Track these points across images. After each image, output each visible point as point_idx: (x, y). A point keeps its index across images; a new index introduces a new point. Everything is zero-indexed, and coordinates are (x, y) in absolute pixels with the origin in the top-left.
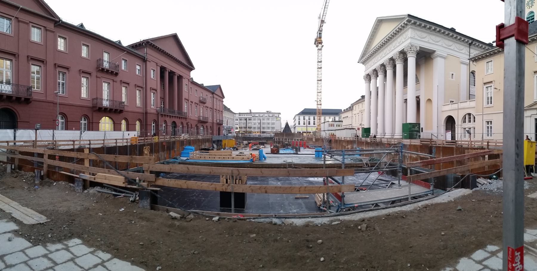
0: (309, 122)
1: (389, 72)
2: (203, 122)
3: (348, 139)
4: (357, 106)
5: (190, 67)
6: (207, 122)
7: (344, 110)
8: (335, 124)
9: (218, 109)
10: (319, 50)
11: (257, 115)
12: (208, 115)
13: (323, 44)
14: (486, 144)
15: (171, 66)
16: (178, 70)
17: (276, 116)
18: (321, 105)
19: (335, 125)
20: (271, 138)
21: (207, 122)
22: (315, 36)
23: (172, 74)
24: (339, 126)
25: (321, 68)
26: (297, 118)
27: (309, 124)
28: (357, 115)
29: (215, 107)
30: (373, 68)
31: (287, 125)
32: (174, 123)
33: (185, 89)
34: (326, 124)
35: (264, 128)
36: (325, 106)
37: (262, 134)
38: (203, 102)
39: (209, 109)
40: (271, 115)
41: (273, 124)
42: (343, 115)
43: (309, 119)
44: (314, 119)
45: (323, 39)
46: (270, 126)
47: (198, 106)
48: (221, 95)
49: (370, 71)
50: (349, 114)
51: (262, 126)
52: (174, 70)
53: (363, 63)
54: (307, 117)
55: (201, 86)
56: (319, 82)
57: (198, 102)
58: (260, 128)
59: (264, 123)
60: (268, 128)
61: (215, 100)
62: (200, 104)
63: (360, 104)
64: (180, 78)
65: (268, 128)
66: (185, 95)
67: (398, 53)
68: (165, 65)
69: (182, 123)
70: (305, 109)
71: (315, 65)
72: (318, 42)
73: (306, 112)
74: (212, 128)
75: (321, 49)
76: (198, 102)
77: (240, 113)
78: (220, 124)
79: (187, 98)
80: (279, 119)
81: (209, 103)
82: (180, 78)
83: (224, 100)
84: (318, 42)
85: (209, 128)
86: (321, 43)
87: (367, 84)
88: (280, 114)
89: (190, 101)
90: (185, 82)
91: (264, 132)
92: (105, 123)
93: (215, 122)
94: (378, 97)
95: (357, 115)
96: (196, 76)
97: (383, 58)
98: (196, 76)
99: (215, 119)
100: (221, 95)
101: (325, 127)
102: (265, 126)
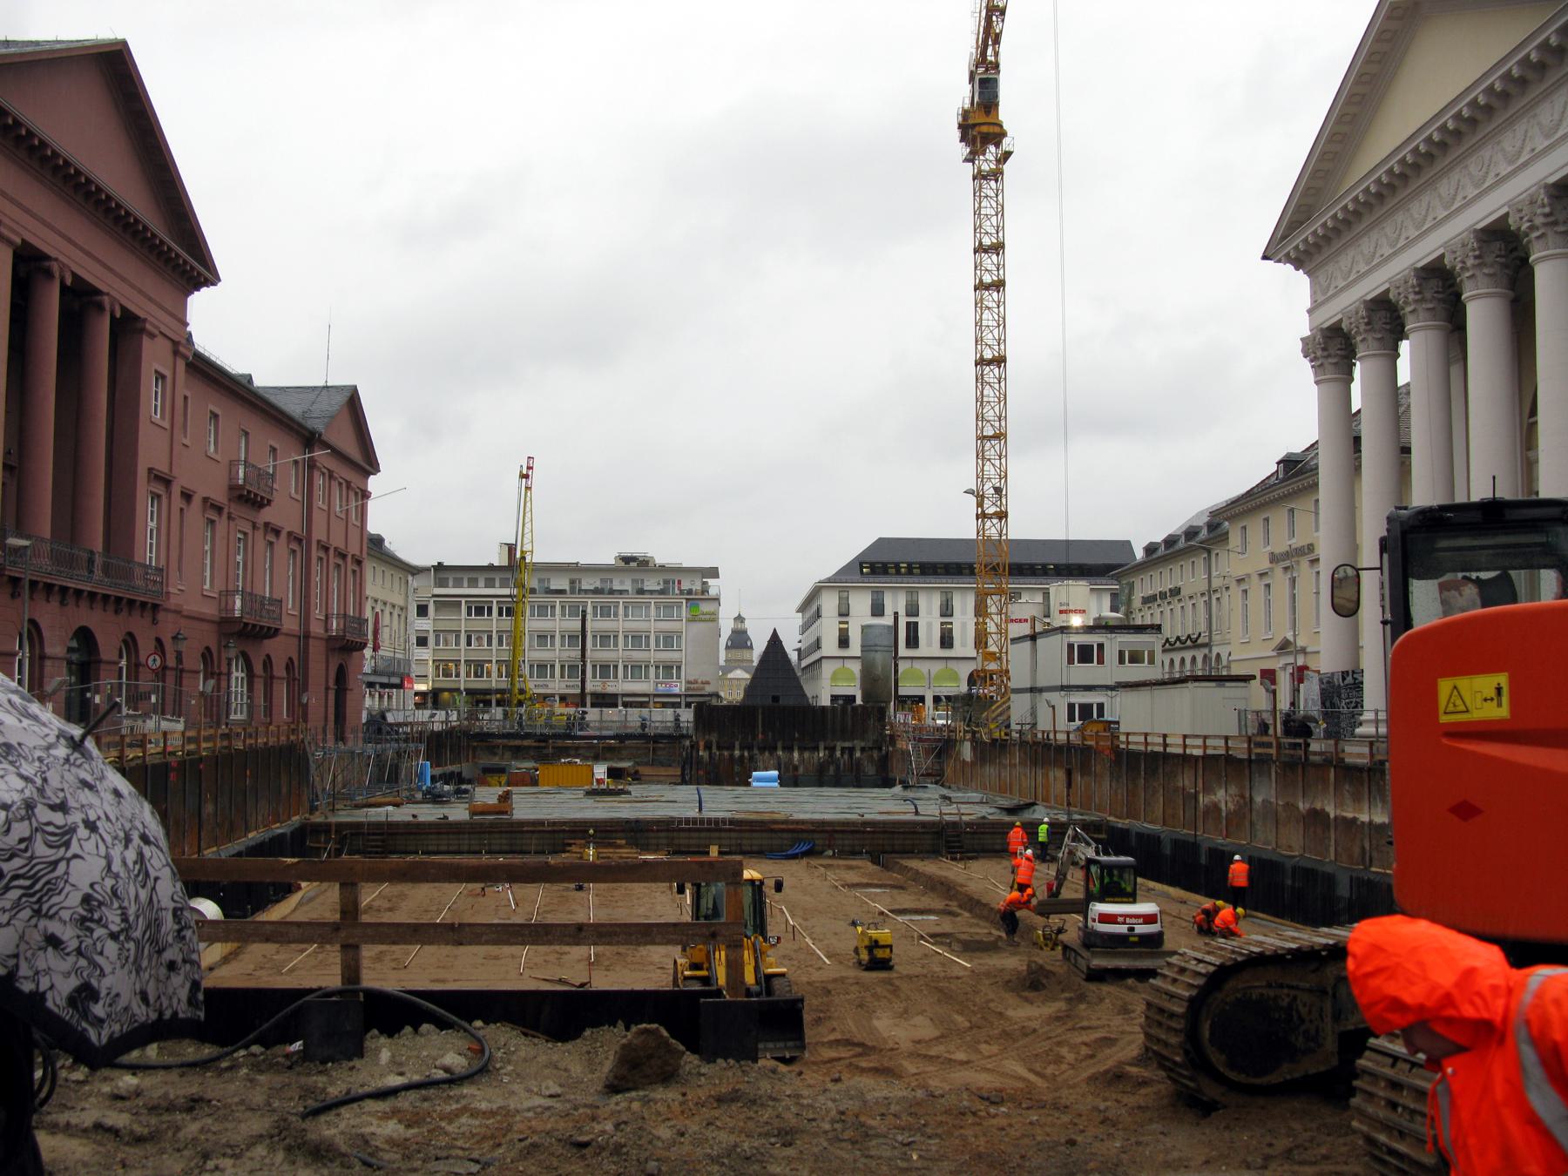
0: (912, 629)
1: (1483, 316)
2: (245, 633)
3: (1216, 747)
4: (1255, 526)
5: (189, 263)
6: (273, 633)
7: (1150, 549)
8: (1113, 644)
9: (337, 541)
10: (980, 176)
11: (560, 583)
12: (276, 579)
13: (1006, 144)
14: (1161, 740)
15: (79, 250)
16: (121, 280)
17: (688, 589)
18: (1002, 515)
19: (1111, 654)
20: (673, 738)
21: (273, 633)
22: (961, 94)
23: (81, 300)
24: (1135, 658)
25: (999, 285)
26: (829, 603)
27: (912, 641)
28: (1256, 587)
29: (319, 533)
30: (1372, 286)
31: (775, 641)
32: (85, 636)
33: (152, 403)
34: (1052, 647)
35: (605, 670)
36: (1029, 522)
37: (593, 714)
38: (249, 499)
39: (282, 546)
40: (652, 584)
41: (668, 640)
42: (1145, 586)
43: (913, 610)
44: (947, 611)
45: (1007, 113)
46: (654, 655)
47: (222, 525)
48: (353, 452)
49: (1349, 301)
50: (1189, 576)
51: (595, 654)
52: (93, 275)
53: (1298, 263)
54: (895, 603)
55: (235, 390)
56: (991, 373)
57: (220, 496)
58: (577, 669)
59: (605, 639)
60: (636, 670)
61: (319, 481)
62: (236, 509)
63: (1279, 517)
64: (127, 327)
65: (636, 670)
66: (151, 451)
67: (1543, 197)
68: (45, 241)
69: (130, 642)
70: (882, 543)
71: (962, 271)
72: (981, 129)
73: (885, 564)
74: (297, 676)
75: (996, 175)
76: (220, 496)
77: (440, 567)
78: (346, 646)
79: (163, 467)
80: (705, 607)
81: (283, 512)
82: (127, 327)
83: (373, 483)
84: (981, 129)
85: (279, 670)
86: (998, 136)
87: (1334, 389)
88: (713, 573)
89: (176, 490)
90: (154, 356)
91: (605, 700)
92: (515, 638)
93: (316, 629)
94: (1357, 469)
95: (1256, 587)
96: (218, 324)
97: (1442, 227)
98: (218, 324)
99: (317, 613)
100: (353, 452)
101: (1044, 663)
102: (619, 654)
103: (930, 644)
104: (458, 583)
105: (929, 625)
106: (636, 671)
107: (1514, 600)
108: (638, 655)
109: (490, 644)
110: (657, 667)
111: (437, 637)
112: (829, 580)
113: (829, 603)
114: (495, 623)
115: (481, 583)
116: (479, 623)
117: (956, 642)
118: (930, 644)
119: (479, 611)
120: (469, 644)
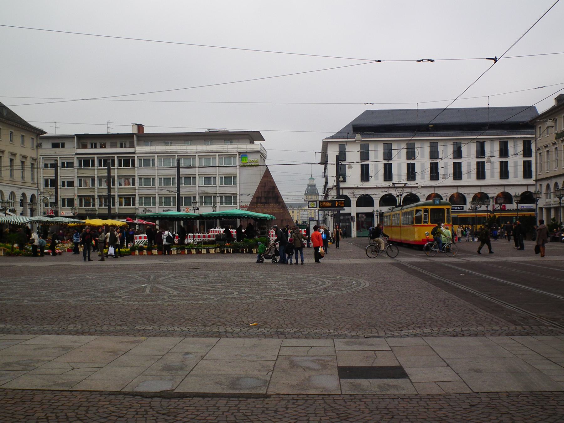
41: (228, 179)
70: (368, 113)
73: (372, 127)
92: (110, 180)
103: (516, 176)
104: (94, 146)
105: (399, 165)
106: (208, 200)
107: (431, 209)
108: (209, 190)
109: (93, 184)
110: (221, 197)
111: (80, 181)
112: (332, 137)
113: (353, 154)
114: (98, 171)
115: (108, 144)
116: (86, 172)
117: (511, 174)
118: (516, 176)
119: (87, 164)
120: (80, 185)
